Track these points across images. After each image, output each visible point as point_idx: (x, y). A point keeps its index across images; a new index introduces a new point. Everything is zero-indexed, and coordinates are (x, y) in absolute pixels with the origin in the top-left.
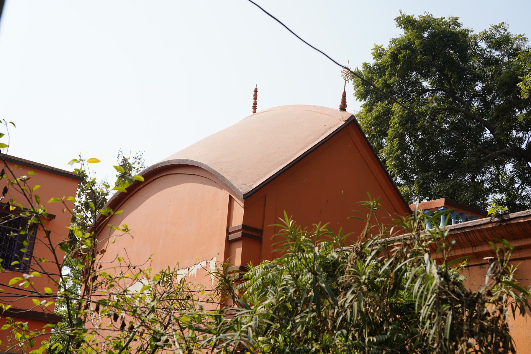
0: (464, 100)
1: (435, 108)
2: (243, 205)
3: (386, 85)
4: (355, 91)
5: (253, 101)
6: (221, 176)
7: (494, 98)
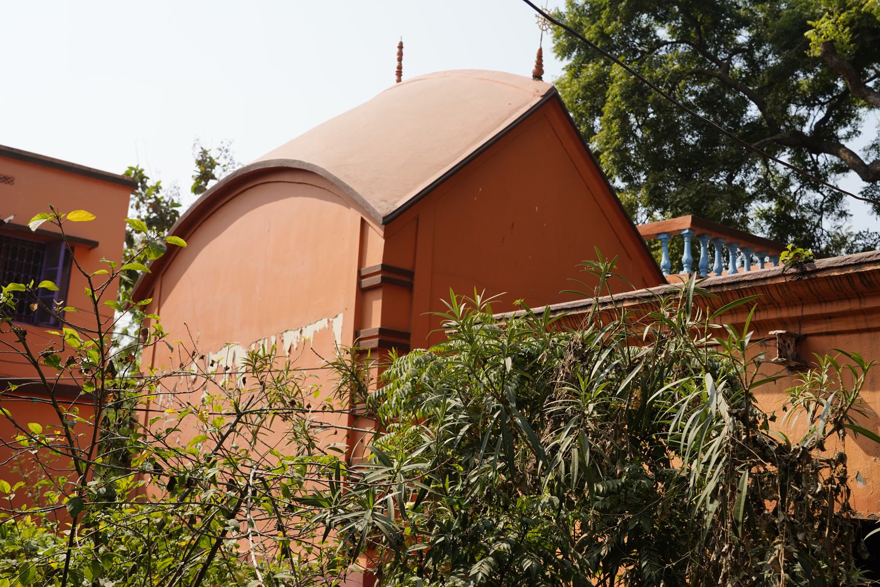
0: (720, 57)
1: (675, 72)
2: (382, 233)
3: (603, 35)
4: (554, 45)
5: (396, 63)
6: (347, 187)
7: (765, 55)
